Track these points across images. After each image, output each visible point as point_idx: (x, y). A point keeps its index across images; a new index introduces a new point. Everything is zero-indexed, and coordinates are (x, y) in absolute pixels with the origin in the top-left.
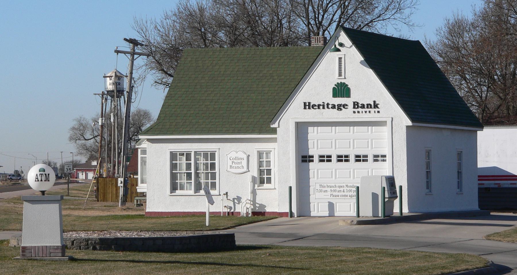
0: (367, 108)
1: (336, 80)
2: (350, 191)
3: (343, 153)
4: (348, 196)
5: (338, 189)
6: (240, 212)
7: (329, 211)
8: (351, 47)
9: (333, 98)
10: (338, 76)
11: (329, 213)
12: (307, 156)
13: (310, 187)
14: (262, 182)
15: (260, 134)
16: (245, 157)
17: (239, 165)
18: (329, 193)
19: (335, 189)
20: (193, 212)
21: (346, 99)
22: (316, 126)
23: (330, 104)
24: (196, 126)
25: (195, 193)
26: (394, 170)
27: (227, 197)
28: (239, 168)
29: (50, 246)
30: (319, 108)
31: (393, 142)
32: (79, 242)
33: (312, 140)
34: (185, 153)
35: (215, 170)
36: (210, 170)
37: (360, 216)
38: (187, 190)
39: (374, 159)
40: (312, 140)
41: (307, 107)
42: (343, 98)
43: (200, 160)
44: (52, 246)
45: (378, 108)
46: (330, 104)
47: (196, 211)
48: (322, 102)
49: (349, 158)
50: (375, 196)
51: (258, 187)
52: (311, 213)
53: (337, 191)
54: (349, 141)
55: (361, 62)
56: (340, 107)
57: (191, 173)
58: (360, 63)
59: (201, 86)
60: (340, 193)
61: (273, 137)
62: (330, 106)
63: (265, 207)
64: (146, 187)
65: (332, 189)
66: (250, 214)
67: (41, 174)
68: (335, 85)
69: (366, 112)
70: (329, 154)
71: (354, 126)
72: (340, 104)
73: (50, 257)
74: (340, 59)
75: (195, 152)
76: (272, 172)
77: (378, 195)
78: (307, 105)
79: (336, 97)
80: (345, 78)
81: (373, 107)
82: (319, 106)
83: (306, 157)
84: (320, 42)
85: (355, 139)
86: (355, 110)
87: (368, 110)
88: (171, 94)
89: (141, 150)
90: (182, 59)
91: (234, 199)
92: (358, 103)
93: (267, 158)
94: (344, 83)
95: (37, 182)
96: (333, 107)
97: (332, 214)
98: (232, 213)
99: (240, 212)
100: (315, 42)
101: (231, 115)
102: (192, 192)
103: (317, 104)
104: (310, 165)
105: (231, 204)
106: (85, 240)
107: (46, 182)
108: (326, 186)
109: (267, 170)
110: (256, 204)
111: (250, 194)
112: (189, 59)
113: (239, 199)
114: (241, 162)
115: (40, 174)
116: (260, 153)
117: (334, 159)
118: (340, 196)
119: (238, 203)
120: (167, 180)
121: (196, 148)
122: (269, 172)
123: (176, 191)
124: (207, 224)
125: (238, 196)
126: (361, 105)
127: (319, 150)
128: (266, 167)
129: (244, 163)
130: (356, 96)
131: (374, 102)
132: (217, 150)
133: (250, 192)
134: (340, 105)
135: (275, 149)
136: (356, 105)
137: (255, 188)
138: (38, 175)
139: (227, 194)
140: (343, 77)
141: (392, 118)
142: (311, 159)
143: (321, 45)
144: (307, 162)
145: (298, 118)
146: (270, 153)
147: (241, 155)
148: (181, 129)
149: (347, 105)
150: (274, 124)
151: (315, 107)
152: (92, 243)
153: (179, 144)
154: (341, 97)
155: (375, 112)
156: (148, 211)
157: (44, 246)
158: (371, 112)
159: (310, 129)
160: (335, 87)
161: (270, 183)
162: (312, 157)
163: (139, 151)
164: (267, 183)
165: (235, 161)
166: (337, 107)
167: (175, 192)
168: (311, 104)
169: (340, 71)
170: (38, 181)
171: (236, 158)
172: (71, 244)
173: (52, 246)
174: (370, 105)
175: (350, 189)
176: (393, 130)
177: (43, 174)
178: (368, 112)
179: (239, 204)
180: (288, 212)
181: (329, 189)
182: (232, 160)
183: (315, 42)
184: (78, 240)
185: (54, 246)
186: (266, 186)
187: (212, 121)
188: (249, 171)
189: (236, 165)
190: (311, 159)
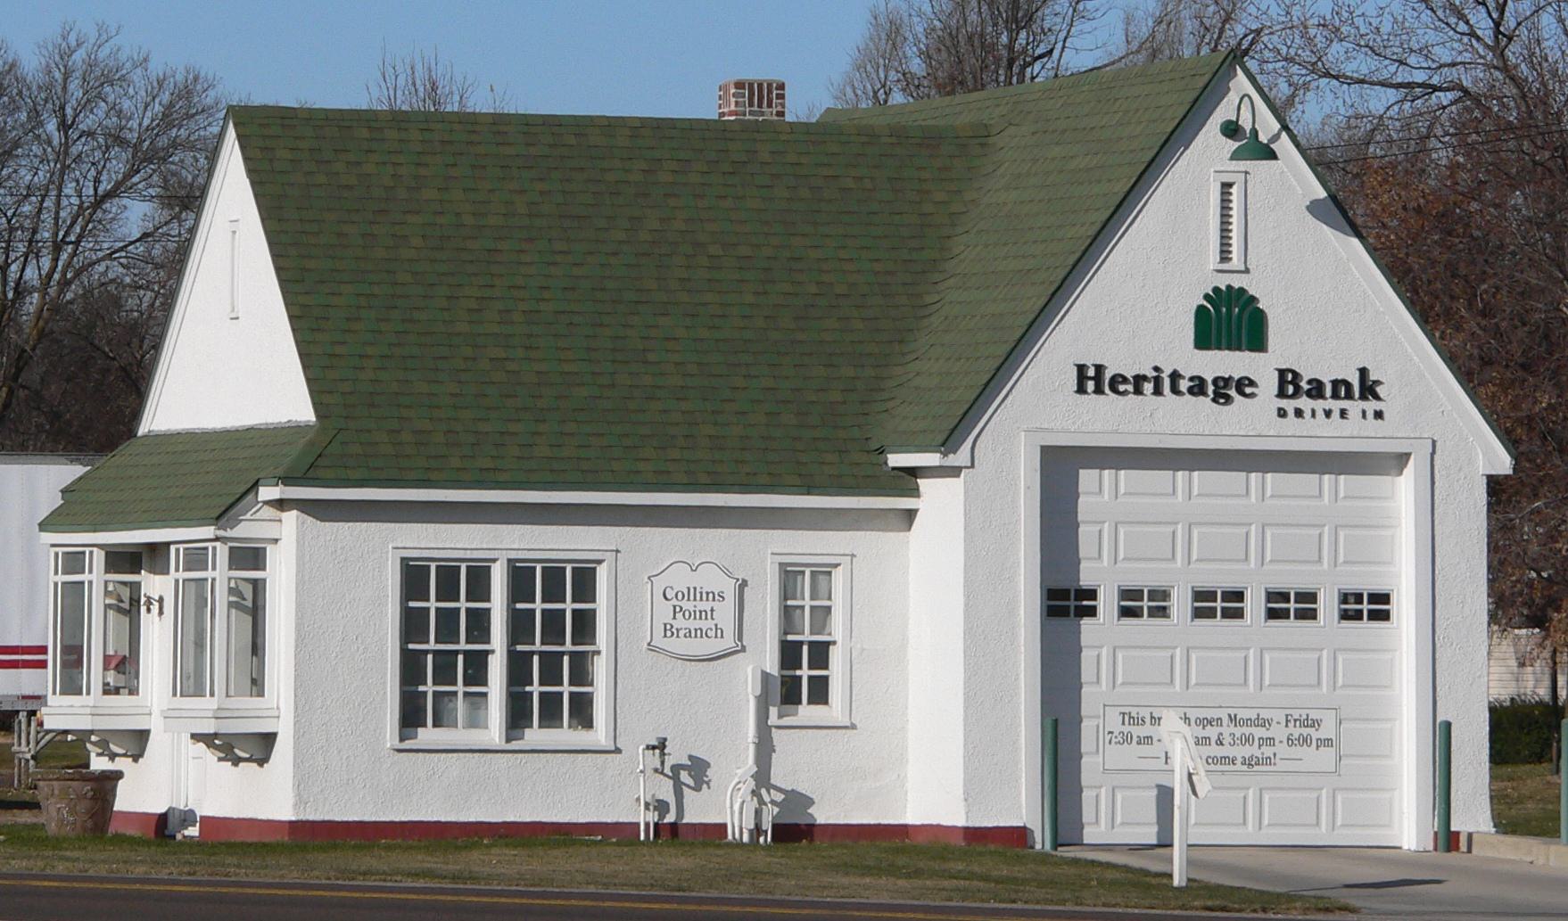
0: (1335, 396)
1: (1205, 276)
2: (1247, 740)
3: (1292, 581)
4: (1239, 760)
6: (724, 826)
9: (1196, 351)
14: (790, 694)
15: (808, 494)
17: (704, 624)
21: (1247, 356)
22: (1110, 468)
23: (1184, 378)
28: (701, 633)
30: (1138, 391)
34: (433, 566)
36: (574, 643)
39: (1197, 608)
41: (1091, 385)
42: (1237, 353)
43: (799, 595)
45: (1377, 397)
46: (1184, 378)
48: (1153, 365)
51: (780, 716)
52: (1086, 831)
53: (1135, 739)
54: (1170, 529)
55: (1315, 208)
58: (1308, 208)
61: (795, 506)
62: (1184, 385)
63: (810, 802)
68: (1207, 297)
69: (1328, 414)
70: (1305, 585)
71: (1192, 470)
72: (1227, 376)
76: (836, 655)
78: (1091, 378)
81: (1357, 395)
82: (1139, 380)
84: (770, 105)
85: (1195, 524)
86: (1284, 403)
87: (1336, 405)
89: (231, 548)
91: (676, 769)
92: (1295, 374)
94: (1242, 291)
96: (1196, 390)
99: (724, 826)
100: (751, 104)
104: (1083, 627)
105: (666, 791)
108: (1148, 720)
109: (811, 644)
113: (698, 768)
114: (712, 610)
117: (1254, 604)
119: (692, 784)
121: (516, 546)
122: (820, 654)
123: (420, 730)
126: (1310, 382)
127: (1119, 565)
128: (812, 633)
129: (725, 614)
130: (1285, 348)
131: (1363, 372)
135: (617, 551)
136: (1291, 382)
141: (1434, 443)
142: (1085, 603)
147: (711, 580)
149: (1252, 383)
150: (955, 453)
151: (1122, 388)
154: (1229, 348)
155: (1364, 413)
158: (1351, 414)
159: (1087, 477)
162: (1092, 594)
164: (810, 702)
166: (1211, 389)
167: (522, 738)
168: (1108, 375)
171: (692, 593)
174: (1348, 385)
175: (1247, 730)
178: (1336, 414)
179: (697, 788)
182: (674, 602)
183: (751, 104)
186: (807, 712)
188: (743, 649)
190: (1085, 603)
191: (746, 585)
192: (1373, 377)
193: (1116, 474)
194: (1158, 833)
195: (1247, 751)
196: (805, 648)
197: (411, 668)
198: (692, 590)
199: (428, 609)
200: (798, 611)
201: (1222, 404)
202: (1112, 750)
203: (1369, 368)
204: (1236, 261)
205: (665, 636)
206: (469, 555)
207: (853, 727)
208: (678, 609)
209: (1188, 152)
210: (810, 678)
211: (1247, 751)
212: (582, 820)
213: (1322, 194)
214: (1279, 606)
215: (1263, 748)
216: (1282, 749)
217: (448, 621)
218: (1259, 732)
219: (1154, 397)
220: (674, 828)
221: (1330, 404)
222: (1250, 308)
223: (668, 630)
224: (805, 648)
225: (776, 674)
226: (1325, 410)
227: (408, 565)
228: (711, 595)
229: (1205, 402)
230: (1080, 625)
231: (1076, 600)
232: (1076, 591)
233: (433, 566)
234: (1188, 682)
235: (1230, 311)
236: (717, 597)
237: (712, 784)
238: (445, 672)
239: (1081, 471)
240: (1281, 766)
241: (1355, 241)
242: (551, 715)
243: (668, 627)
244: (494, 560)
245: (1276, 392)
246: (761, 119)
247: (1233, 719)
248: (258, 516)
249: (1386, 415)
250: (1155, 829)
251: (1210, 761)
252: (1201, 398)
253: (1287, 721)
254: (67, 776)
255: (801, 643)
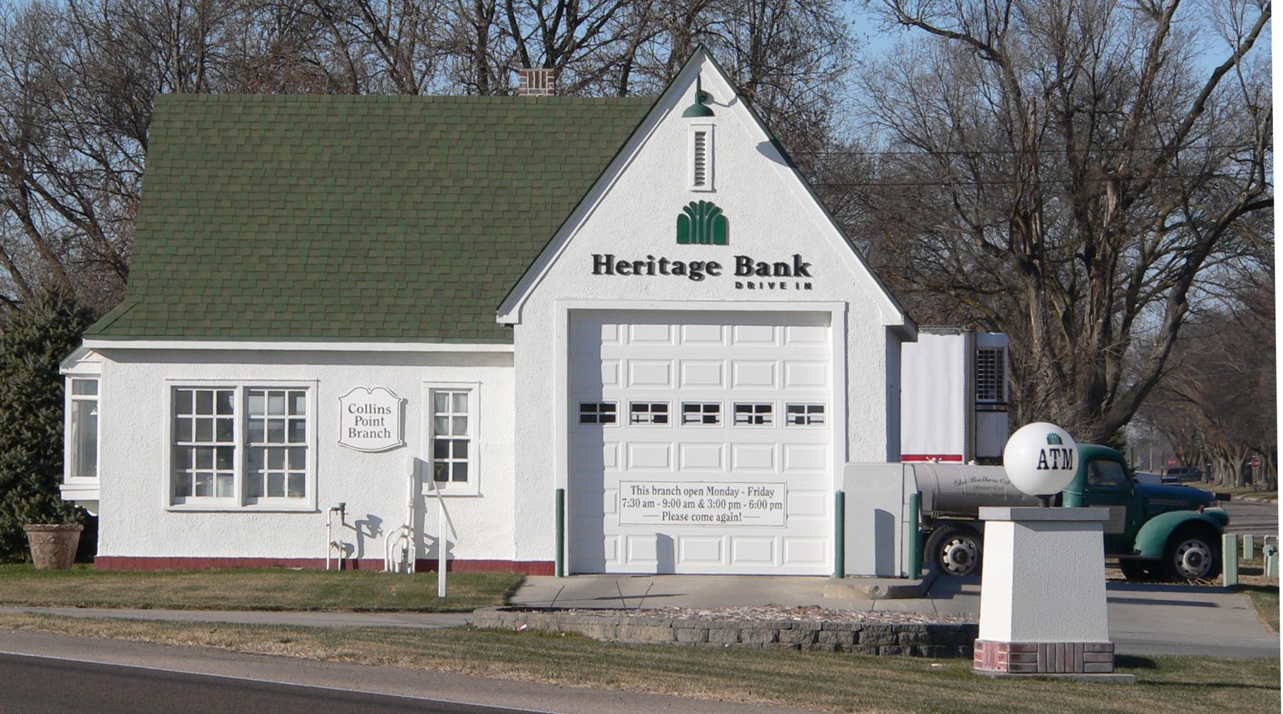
0: (777, 273)
1: (685, 194)
4: (715, 518)
5: (684, 498)
6: (383, 560)
7: (658, 558)
8: (732, 103)
9: (678, 245)
10: (693, 183)
11: (658, 566)
12: (595, 405)
13: (604, 491)
14: (440, 475)
15: (442, 342)
16: (394, 405)
17: (377, 429)
18: (659, 510)
19: (676, 497)
20: (240, 559)
23: (669, 263)
24: (249, 316)
25: (243, 506)
26: (850, 448)
27: (343, 519)
29: (1084, 644)
30: (637, 272)
31: (849, 369)
32: (875, 634)
33: (664, 360)
34: (194, 391)
35: (304, 441)
36: (290, 441)
37: (846, 572)
38: (217, 496)
40: (664, 360)
41: (603, 269)
44: (1088, 644)
45: (807, 274)
46: (669, 263)
47: (246, 555)
49: (304, 413)
50: (884, 521)
51: (431, 488)
54: (718, 364)
55: (761, 148)
56: (696, 271)
57: (233, 448)
59: (232, 201)
60: (690, 509)
62: (669, 268)
64: (98, 487)
65: (669, 498)
66: (411, 565)
67: (1055, 450)
68: (685, 209)
69: (772, 286)
71: (630, 324)
72: (699, 261)
73: (1084, 673)
74: (699, 136)
75: (245, 388)
76: (471, 449)
77: (893, 517)
78: (604, 264)
79: (687, 243)
80: (714, 190)
81: (793, 273)
82: (637, 265)
83: (592, 407)
84: (544, 86)
86: (740, 279)
87: (777, 280)
88: (150, 223)
90: (157, 123)
91: (359, 523)
92: (748, 260)
93: (456, 409)
94: (711, 204)
95: (1043, 471)
97: (666, 569)
98: (355, 562)
99: (383, 560)
100: (531, 86)
101: (344, 285)
102: (235, 501)
103: (631, 262)
104: (604, 429)
105: (352, 538)
106: (889, 631)
107: (1065, 471)
108: (651, 491)
109: (455, 441)
110: (425, 538)
111: (409, 509)
112: (179, 124)
113: (374, 523)
114: (382, 419)
115: (1051, 450)
116: (435, 394)
118: (690, 518)
119: (370, 533)
120: (160, 468)
122: (462, 448)
123: (187, 498)
124: (442, 592)
125: (372, 516)
126: (758, 265)
129: (392, 422)
130: (742, 241)
131: (797, 258)
132: (313, 385)
133: (408, 504)
134: (700, 265)
135: (318, 381)
136: (744, 265)
137: (423, 493)
138: (1047, 453)
139: (342, 507)
140: (707, 186)
141: (847, 304)
142: (607, 413)
143: (547, 94)
144: (596, 422)
145: (576, 299)
146: (466, 395)
148: (207, 323)
149: (717, 266)
151: (625, 270)
152: (908, 637)
153: (199, 366)
154: (701, 243)
156: (104, 555)
157: (1069, 643)
159: (608, 330)
160: (685, 213)
161: (465, 479)
162: (612, 407)
163: (68, 382)
164: (454, 480)
165: (365, 416)
166: (688, 270)
167: (184, 503)
168: (616, 262)
169: (700, 171)
170: (1046, 468)
171: (369, 408)
172: (850, 639)
173: (1088, 644)
174: (786, 266)
175: (721, 498)
176: (849, 338)
177: (1058, 450)
178: (777, 286)
179: (373, 536)
180: (554, 562)
181: (658, 499)
182: (357, 414)
183: (531, 86)
184: (871, 629)
185: (1094, 645)
186: (451, 486)
187: (291, 301)
188: (405, 445)
189: (369, 429)
190: (607, 413)
191: (407, 403)
192: (804, 261)
193: (680, 328)
194: (658, 566)
195: (721, 511)
196: (451, 444)
197: (180, 458)
198: (368, 407)
199: (212, 419)
200: (445, 420)
201: (697, 280)
202: (625, 511)
203: (801, 254)
204: (707, 186)
205: (350, 436)
206: (217, 384)
207: (480, 496)
208: (359, 419)
209: (672, 112)
210: (454, 464)
211: (721, 511)
212: (293, 557)
213: (766, 139)
214: (710, 413)
215: (732, 510)
216: (745, 511)
217: (204, 426)
218: (729, 499)
219: (648, 276)
220: (356, 563)
221: (773, 279)
222: (716, 216)
223: (352, 433)
224: (451, 444)
225: (427, 460)
226: (769, 284)
227: (177, 391)
228: (381, 410)
229: (684, 279)
230: (602, 428)
231: (601, 411)
232: (601, 405)
233: (194, 391)
234: (679, 465)
235: (701, 218)
236: (385, 411)
237: (383, 533)
238: (204, 461)
239: (604, 326)
240: (744, 521)
241: (789, 169)
242: (276, 491)
243: (352, 430)
244: (235, 387)
245: (593, 271)
246: (537, 95)
247: (711, 490)
248: (90, 359)
249: (813, 286)
250: (656, 563)
251: (694, 518)
252: (682, 276)
253: (749, 492)
254: (36, 529)
255: (448, 441)
